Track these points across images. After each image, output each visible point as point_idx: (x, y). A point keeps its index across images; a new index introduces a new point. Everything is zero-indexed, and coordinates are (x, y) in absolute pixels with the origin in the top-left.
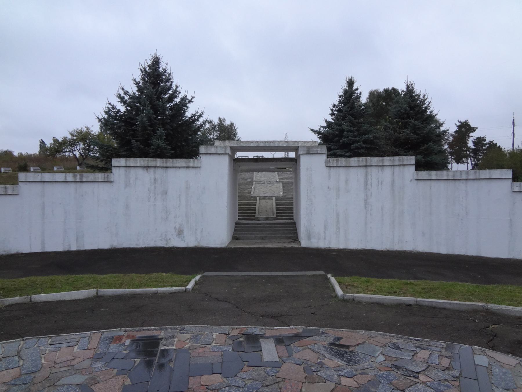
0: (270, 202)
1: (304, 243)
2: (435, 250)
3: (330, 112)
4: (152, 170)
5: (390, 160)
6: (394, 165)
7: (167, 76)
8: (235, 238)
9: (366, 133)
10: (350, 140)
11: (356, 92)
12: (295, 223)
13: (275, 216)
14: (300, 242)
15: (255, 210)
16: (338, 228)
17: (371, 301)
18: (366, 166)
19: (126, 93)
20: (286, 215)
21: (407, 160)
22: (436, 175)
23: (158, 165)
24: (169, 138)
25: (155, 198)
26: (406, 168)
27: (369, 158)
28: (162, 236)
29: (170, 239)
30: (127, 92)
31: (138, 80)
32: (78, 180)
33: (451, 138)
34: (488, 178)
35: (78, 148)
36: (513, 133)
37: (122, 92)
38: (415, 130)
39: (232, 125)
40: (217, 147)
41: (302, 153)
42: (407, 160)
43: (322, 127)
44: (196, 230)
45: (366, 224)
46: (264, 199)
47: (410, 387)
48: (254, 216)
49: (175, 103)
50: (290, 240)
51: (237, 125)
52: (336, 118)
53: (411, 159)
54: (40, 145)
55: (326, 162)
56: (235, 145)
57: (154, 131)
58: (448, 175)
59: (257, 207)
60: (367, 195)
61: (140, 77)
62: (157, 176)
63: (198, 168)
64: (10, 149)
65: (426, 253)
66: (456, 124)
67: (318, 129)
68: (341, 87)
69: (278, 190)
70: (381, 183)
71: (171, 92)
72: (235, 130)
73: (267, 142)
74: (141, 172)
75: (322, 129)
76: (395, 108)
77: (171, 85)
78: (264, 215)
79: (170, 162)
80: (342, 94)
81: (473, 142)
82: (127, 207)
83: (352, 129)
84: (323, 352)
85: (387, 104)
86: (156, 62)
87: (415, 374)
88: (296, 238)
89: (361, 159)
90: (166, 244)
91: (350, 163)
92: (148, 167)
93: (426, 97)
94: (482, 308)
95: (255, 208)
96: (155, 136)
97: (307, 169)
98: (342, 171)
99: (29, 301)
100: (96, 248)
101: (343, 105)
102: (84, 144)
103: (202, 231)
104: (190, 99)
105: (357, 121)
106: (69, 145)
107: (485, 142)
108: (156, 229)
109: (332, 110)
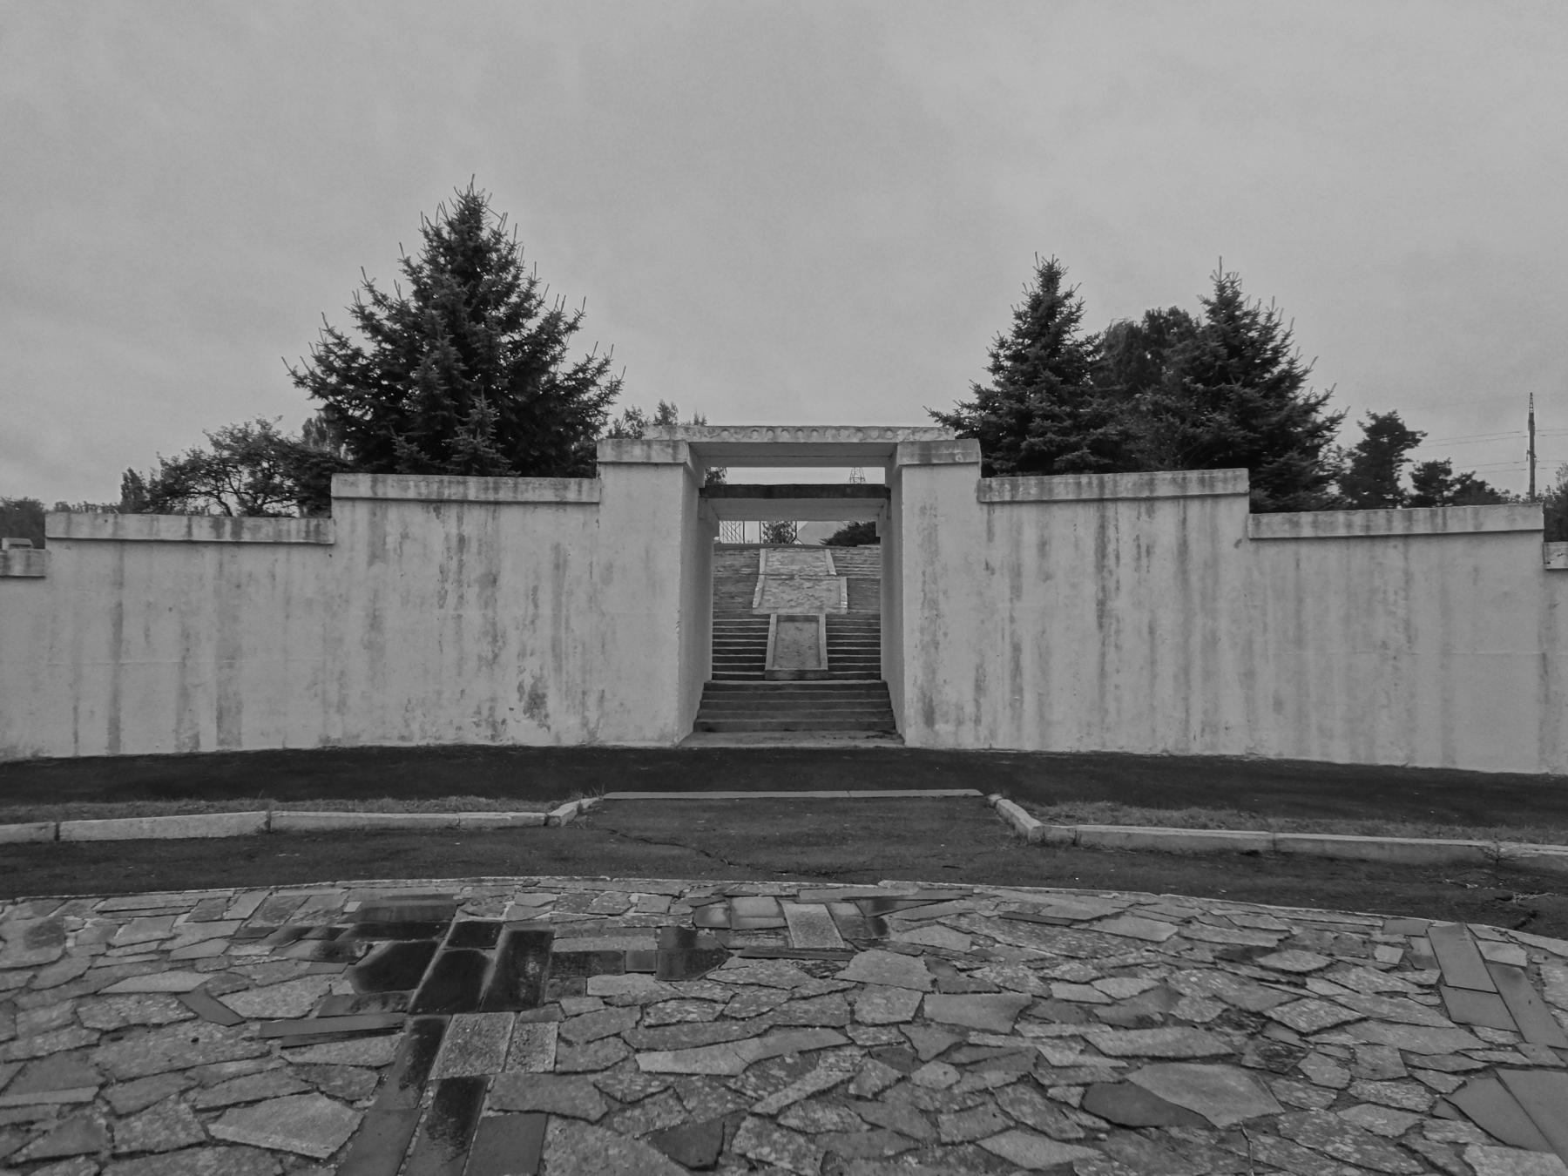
0: (809, 628)
1: (914, 735)
2: (1315, 753)
3: (990, 362)
4: (452, 513)
5: (1174, 480)
6: (1185, 498)
8: (702, 727)
9: (1100, 420)
10: (1051, 441)
11: (1067, 302)
12: (885, 686)
13: (825, 666)
14: (900, 736)
15: (764, 652)
16: (1018, 690)
17: (1130, 845)
18: (1101, 500)
19: (380, 301)
20: (859, 664)
21: (1225, 481)
22: (1315, 525)
23: (472, 496)
25: (461, 597)
26: (1223, 505)
27: (1108, 477)
28: (479, 712)
29: (504, 722)
30: (384, 297)
31: (415, 262)
32: (227, 538)
33: (1349, 463)
34: (1470, 529)
35: (236, 484)
36: (1532, 453)
37: (367, 300)
38: (1246, 414)
40: (649, 443)
41: (906, 461)
42: (1225, 481)
43: (964, 406)
44: (584, 693)
45: (1103, 674)
46: (791, 619)
47: (1281, 1004)
48: (762, 668)
49: (525, 332)
50: (871, 733)
52: (1008, 379)
53: (1235, 479)
54: (124, 488)
55: (980, 490)
56: (704, 440)
57: (462, 410)
58: (1349, 526)
60: (1104, 589)
61: (424, 256)
62: (469, 529)
63: (594, 508)
64: (31, 498)
65: (1287, 761)
66: (1361, 424)
67: (952, 413)
68: (1022, 289)
69: (835, 597)
70: (1148, 553)
71: (514, 299)
73: (800, 429)
74: (417, 515)
75: (965, 413)
76: (1183, 351)
77: (516, 277)
79: (507, 487)
80: (1024, 308)
81: (1415, 477)
82: (375, 622)
83: (1056, 409)
84: (986, 932)
85: (1156, 355)
86: (471, 213)
87: (1293, 979)
88: (889, 728)
89: (1084, 479)
90: (493, 737)
91: (1051, 491)
92: (441, 501)
93: (1275, 319)
94: (1480, 856)
95: (765, 644)
96: (463, 424)
97: (923, 510)
98: (1028, 515)
99: (51, 836)
100: (276, 745)
101: (1027, 342)
102: (253, 474)
103: (602, 698)
104: (570, 320)
106: (208, 474)
107: (1450, 478)
109: (996, 356)
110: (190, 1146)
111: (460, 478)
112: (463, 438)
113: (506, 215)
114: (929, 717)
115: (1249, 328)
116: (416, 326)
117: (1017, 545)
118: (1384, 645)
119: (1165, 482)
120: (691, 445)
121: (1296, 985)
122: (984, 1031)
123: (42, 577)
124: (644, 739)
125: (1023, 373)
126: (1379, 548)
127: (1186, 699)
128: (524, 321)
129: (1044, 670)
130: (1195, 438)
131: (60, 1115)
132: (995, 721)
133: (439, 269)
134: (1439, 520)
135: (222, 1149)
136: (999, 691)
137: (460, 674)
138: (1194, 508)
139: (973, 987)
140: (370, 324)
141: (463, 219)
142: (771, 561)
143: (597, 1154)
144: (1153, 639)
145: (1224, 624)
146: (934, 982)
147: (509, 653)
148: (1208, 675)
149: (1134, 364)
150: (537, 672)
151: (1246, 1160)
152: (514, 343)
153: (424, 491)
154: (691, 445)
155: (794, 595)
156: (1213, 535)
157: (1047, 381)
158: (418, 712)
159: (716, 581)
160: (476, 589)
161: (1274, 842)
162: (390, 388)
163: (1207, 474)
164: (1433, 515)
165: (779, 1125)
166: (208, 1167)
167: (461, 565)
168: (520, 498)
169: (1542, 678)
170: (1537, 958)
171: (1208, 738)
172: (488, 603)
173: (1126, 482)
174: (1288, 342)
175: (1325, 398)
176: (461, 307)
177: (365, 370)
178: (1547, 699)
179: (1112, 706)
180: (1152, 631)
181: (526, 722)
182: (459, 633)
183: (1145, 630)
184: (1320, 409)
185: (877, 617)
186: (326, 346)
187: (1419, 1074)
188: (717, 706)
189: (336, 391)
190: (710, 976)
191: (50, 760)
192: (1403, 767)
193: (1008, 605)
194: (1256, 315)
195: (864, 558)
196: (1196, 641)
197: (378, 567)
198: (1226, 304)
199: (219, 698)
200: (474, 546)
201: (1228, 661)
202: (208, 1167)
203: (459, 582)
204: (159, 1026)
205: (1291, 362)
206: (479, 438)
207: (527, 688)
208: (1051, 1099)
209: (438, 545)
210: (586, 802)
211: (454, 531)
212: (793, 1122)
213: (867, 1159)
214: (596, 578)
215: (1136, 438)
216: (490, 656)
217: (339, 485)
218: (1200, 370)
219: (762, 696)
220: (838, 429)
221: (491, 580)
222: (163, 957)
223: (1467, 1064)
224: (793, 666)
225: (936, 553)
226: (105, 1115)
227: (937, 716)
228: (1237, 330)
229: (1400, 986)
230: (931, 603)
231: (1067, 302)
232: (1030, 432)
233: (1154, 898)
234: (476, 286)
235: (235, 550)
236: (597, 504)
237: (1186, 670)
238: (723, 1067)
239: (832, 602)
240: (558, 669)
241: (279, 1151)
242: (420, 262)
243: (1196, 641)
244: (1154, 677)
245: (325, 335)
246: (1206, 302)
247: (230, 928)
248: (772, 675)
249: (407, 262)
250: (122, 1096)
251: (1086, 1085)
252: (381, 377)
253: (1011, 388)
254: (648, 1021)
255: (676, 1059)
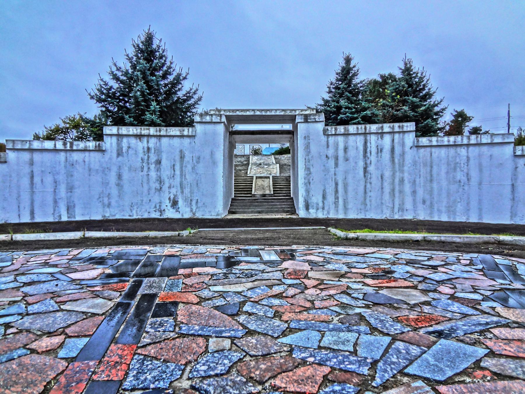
1: (302, 213)
3: (328, 90)
7: (161, 52)
8: (231, 212)
9: (365, 109)
10: (348, 116)
11: (354, 69)
15: (252, 188)
16: (337, 198)
17: (376, 239)
19: (119, 69)
20: (283, 191)
23: (152, 133)
24: (162, 114)
25: (149, 168)
28: (155, 207)
29: (164, 210)
30: (120, 68)
32: (68, 148)
36: (509, 124)
40: (212, 115)
41: (300, 121)
43: (319, 105)
45: (365, 192)
46: (261, 177)
48: (251, 194)
49: (169, 80)
57: (148, 106)
58: (449, 141)
60: (366, 164)
62: (151, 145)
66: (452, 114)
68: (339, 64)
70: (381, 151)
71: (165, 68)
74: (133, 141)
76: (393, 86)
77: (165, 61)
81: (469, 131)
82: (120, 177)
83: (350, 105)
86: (149, 39)
93: (424, 74)
94: (493, 240)
96: (148, 111)
97: (305, 137)
98: (341, 139)
99: (10, 239)
101: (340, 83)
102: (77, 132)
103: (197, 202)
105: (355, 98)
107: (481, 132)
108: (150, 200)
109: (329, 88)
110: (54, 311)
111: (148, 128)
112: (148, 116)
113: (161, 39)
114: (307, 208)
115: (415, 78)
116: (131, 78)
117: (337, 149)
118: (460, 181)
119: (387, 127)
120: (226, 116)
121: (434, 269)
122: (329, 280)
123: (6, 162)
124: (211, 215)
125: (339, 93)
126: (459, 149)
127: (393, 200)
128: (168, 76)
129: (346, 191)
130: (397, 115)
131: (9, 304)
132: (329, 208)
133: (139, 58)
134: (479, 139)
135: (65, 312)
136: (331, 198)
137: (149, 194)
138: (397, 136)
139: (325, 270)
140: (116, 78)
141: (147, 41)
142: (254, 159)
143: (196, 312)
144: (382, 181)
145: (406, 175)
146: (311, 268)
147: (165, 187)
148: (401, 192)
149: (376, 93)
150: (175, 193)
151: (420, 312)
152: (165, 84)
153: (135, 132)
154: (226, 116)
155: (261, 170)
156: (403, 145)
157: (347, 96)
158: (135, 207)
159: (235, 167)
160: (153, 165)
161: (424, 237)
162: (123, 100)
163: (401, 124)
164: (477, 137)
165: (259, 304)
166: (60, 317)
167: (148, 157)
168: (168, 134)
169: (512, 192)
170: (514, 263)
171: (400, 213)
172: (158, 170)
173: (374, 128)
174: (428, 82)
175: (441, 102)
176: (147, 71)
177: (114, 93)
178: (513, 199)
179: (368, 204)
180: (382, 178)
181: (172, 210)
182: (148, 180)
183: (380, 177)
184: (439, 105)
185: (290, 177)
186: (101, 85)
187: (477, 291)
188: (236, 206)
189: (104, 101)
190: (234, 267)
191: (10, 224)
192: (465, 222)
193: (334, 169)
194: (417, 73)
195: (285, 158)
196: (397, 181)
197: (120, 158)
198: (407, 71)
199: (67, 202)
200: (153, 151)
201: (407, 188)
202: (60, 317)
203: (148, 164)
204: (45, 281)
205: (429, 89)
206: (154, 116)
207: (172, 199)
208: (353, 297)
209: (140, 150)
210: (192, 231)
211: (146, 146)
212: (264, 303)
213: (290, 312)
214: (194, 161)
215: (377, 116)
216: (159, 188)
217: (107, 130)
218: (398, 92)
219: (251, 202)
220: (276, 110)
221: (159, 162)
222: (46, 264)
223: (494, 288)
224: (261, 193)
225: (309, 152)
226: (25, 304)
227: (310, 207)
228: (411, 78)
229: (469, 269)
230: (308, 169)
231: (354, 69)
232: (341, 113)
233: (385, 249)
234: (151, 65)
235: (71, 153)
236: (194, 136)
237: (393, 190)
238: (240, 290)
239: (274, 172)
240: (182, 192)
241: (85, 312)
242: (132, 56)
243: (397, 181)
244: (383, 193)
245: (100, 81)
246: (401, 69)
247: (70, 257)
248: (254, 195)
249: (128, 55)
250: (30, 299)
251: (365, 294)
252: (119, 96)
253: (335, 99)
254: (213, 278)
255: (223, 287)
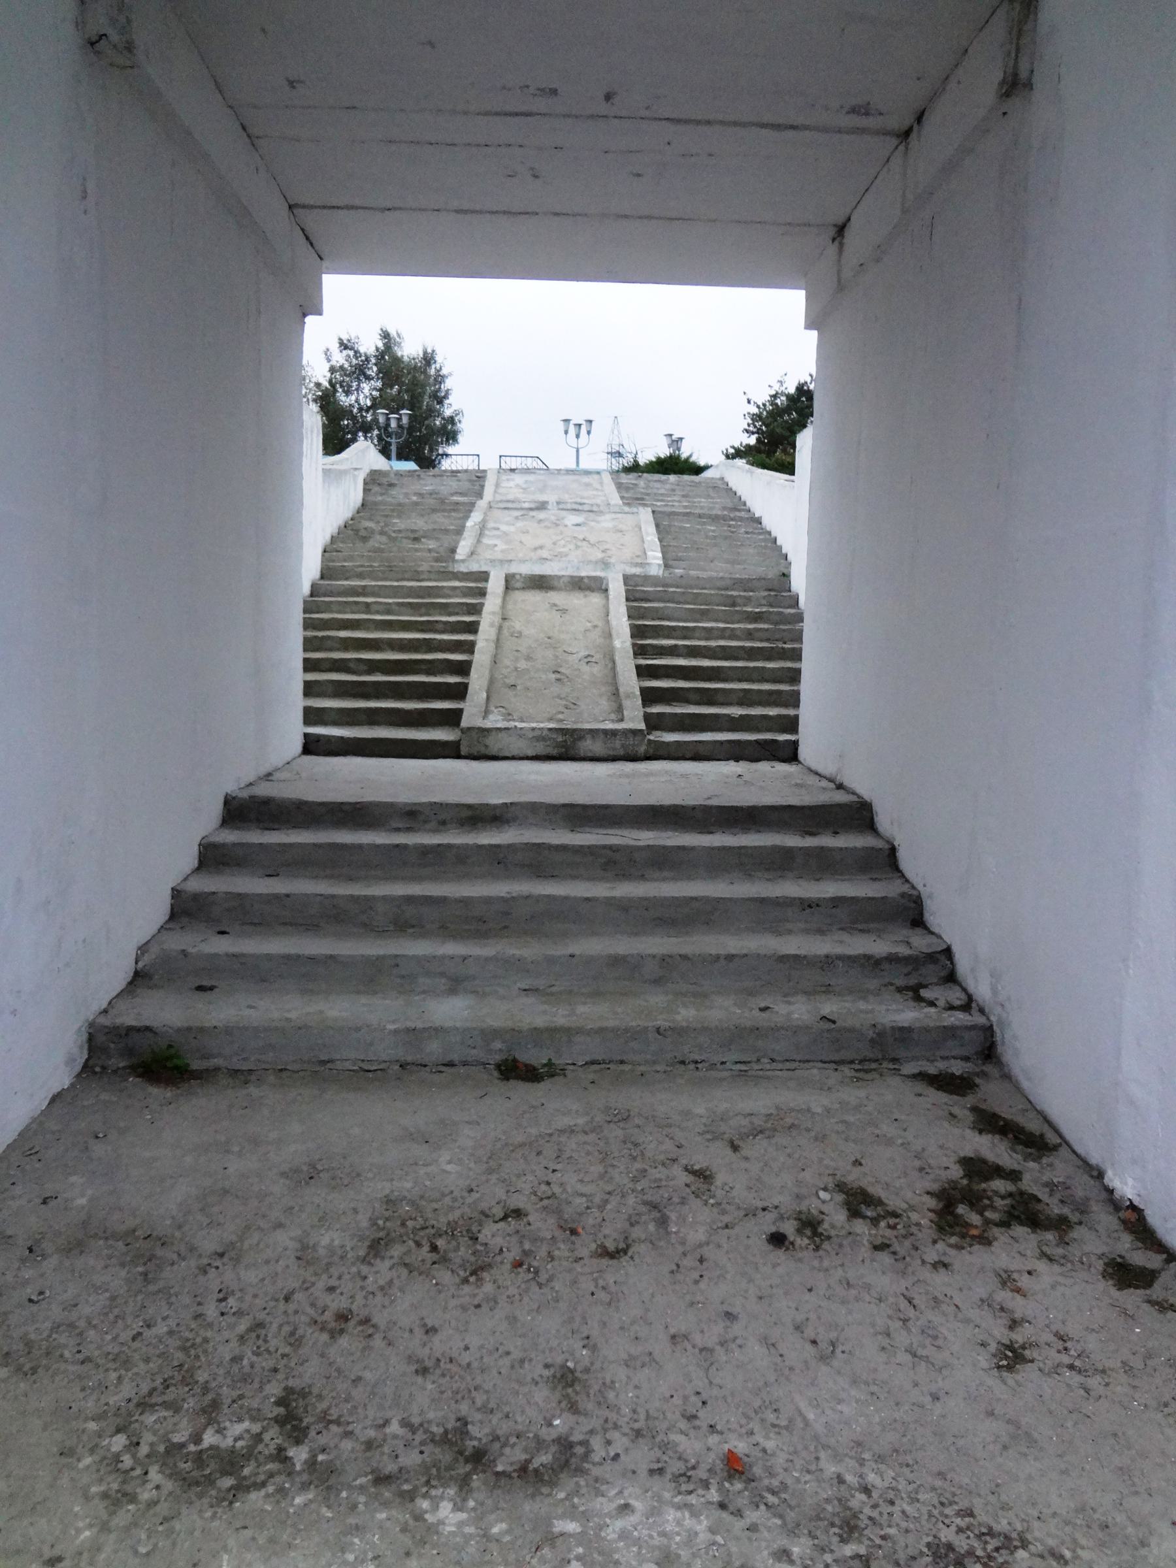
0: (585, 605)
13: (634, 718)
39: (428, 359)
46: (540, 583)
48: (452, 718)
51: (446, 362)
59: (484, 639)
72: (440, 378)
78: (538, 716)
239: (627, 554)
